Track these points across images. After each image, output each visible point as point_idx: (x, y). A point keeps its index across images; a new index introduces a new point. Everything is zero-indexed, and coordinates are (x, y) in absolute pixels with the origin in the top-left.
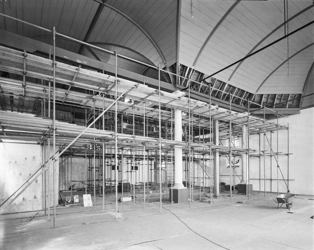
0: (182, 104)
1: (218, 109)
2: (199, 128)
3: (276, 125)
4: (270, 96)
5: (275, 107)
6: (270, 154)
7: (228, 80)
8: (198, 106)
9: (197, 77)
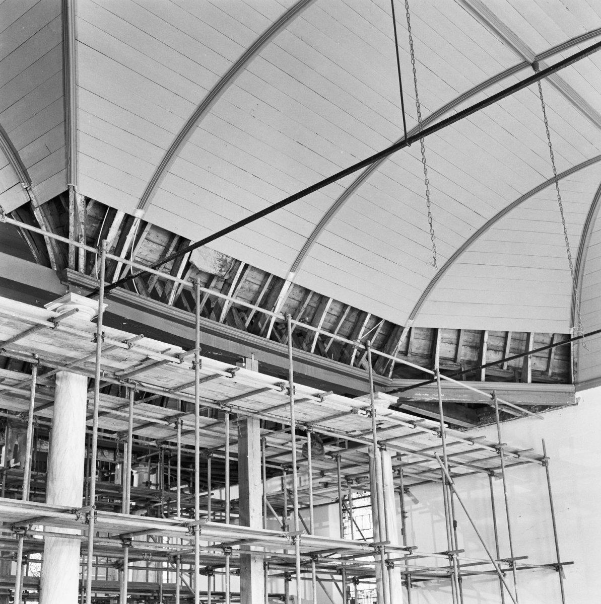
0: (76, 349)
1: (233, 374)
2: (176, 451)
3: (493, 446)
4: (463, 338)
5: (489, 378)
6: (491, 567)
7: (289, 267)
8: (148, 359)
9: (162, 248)
